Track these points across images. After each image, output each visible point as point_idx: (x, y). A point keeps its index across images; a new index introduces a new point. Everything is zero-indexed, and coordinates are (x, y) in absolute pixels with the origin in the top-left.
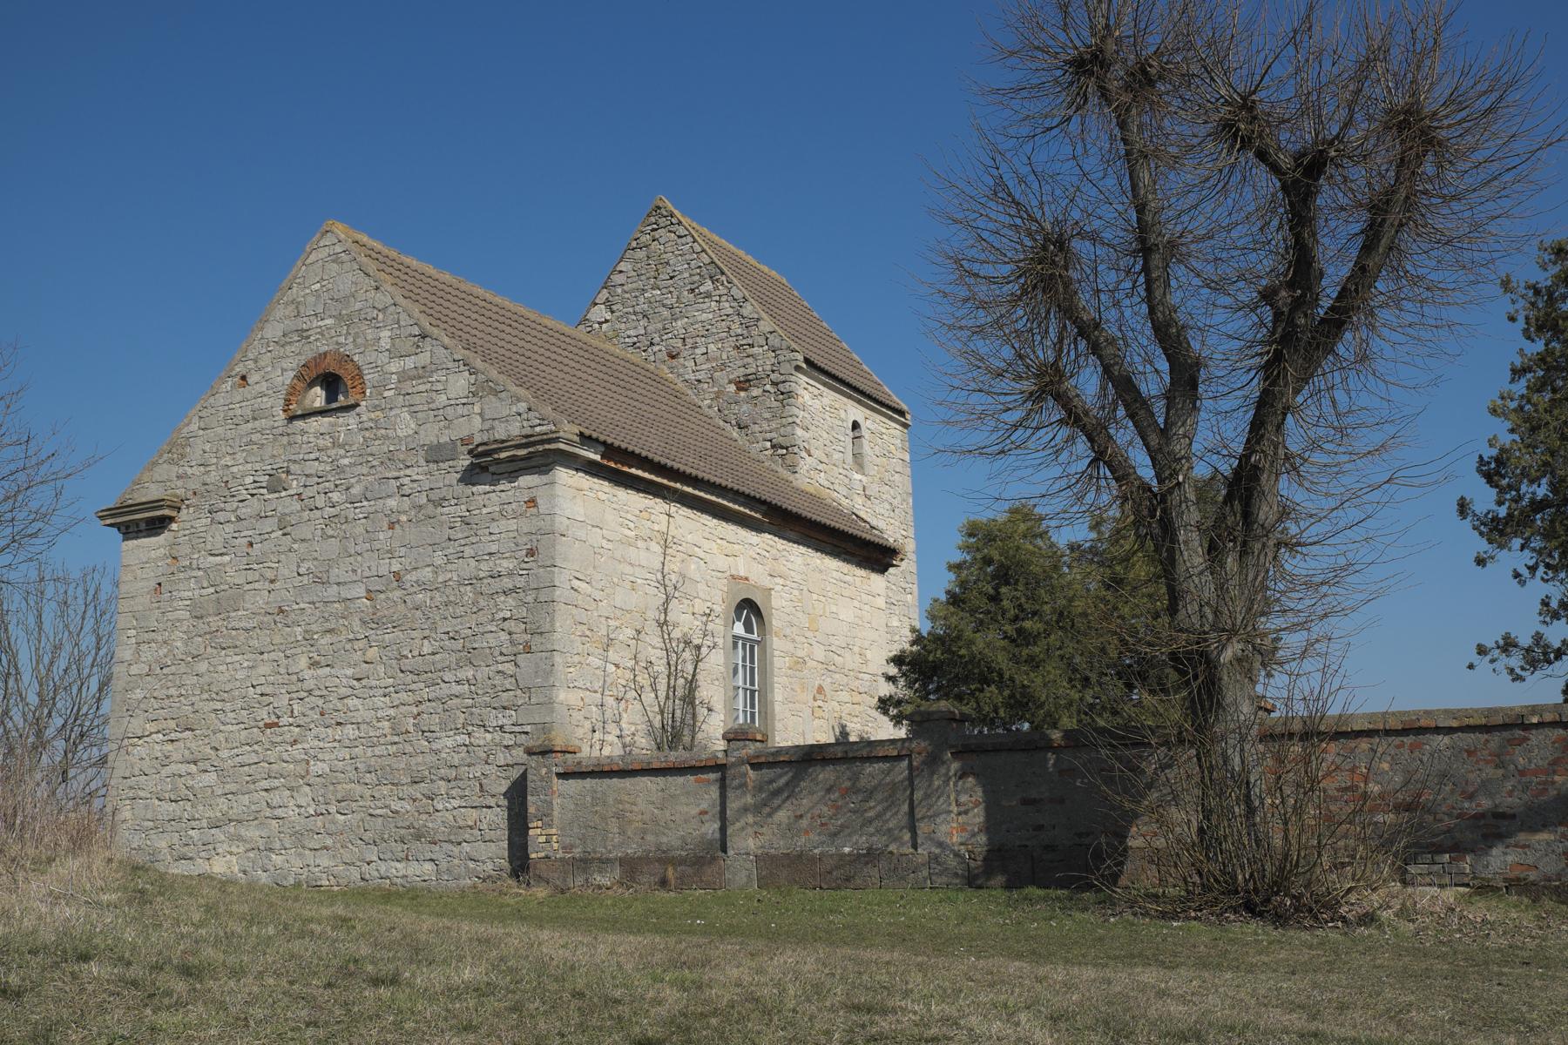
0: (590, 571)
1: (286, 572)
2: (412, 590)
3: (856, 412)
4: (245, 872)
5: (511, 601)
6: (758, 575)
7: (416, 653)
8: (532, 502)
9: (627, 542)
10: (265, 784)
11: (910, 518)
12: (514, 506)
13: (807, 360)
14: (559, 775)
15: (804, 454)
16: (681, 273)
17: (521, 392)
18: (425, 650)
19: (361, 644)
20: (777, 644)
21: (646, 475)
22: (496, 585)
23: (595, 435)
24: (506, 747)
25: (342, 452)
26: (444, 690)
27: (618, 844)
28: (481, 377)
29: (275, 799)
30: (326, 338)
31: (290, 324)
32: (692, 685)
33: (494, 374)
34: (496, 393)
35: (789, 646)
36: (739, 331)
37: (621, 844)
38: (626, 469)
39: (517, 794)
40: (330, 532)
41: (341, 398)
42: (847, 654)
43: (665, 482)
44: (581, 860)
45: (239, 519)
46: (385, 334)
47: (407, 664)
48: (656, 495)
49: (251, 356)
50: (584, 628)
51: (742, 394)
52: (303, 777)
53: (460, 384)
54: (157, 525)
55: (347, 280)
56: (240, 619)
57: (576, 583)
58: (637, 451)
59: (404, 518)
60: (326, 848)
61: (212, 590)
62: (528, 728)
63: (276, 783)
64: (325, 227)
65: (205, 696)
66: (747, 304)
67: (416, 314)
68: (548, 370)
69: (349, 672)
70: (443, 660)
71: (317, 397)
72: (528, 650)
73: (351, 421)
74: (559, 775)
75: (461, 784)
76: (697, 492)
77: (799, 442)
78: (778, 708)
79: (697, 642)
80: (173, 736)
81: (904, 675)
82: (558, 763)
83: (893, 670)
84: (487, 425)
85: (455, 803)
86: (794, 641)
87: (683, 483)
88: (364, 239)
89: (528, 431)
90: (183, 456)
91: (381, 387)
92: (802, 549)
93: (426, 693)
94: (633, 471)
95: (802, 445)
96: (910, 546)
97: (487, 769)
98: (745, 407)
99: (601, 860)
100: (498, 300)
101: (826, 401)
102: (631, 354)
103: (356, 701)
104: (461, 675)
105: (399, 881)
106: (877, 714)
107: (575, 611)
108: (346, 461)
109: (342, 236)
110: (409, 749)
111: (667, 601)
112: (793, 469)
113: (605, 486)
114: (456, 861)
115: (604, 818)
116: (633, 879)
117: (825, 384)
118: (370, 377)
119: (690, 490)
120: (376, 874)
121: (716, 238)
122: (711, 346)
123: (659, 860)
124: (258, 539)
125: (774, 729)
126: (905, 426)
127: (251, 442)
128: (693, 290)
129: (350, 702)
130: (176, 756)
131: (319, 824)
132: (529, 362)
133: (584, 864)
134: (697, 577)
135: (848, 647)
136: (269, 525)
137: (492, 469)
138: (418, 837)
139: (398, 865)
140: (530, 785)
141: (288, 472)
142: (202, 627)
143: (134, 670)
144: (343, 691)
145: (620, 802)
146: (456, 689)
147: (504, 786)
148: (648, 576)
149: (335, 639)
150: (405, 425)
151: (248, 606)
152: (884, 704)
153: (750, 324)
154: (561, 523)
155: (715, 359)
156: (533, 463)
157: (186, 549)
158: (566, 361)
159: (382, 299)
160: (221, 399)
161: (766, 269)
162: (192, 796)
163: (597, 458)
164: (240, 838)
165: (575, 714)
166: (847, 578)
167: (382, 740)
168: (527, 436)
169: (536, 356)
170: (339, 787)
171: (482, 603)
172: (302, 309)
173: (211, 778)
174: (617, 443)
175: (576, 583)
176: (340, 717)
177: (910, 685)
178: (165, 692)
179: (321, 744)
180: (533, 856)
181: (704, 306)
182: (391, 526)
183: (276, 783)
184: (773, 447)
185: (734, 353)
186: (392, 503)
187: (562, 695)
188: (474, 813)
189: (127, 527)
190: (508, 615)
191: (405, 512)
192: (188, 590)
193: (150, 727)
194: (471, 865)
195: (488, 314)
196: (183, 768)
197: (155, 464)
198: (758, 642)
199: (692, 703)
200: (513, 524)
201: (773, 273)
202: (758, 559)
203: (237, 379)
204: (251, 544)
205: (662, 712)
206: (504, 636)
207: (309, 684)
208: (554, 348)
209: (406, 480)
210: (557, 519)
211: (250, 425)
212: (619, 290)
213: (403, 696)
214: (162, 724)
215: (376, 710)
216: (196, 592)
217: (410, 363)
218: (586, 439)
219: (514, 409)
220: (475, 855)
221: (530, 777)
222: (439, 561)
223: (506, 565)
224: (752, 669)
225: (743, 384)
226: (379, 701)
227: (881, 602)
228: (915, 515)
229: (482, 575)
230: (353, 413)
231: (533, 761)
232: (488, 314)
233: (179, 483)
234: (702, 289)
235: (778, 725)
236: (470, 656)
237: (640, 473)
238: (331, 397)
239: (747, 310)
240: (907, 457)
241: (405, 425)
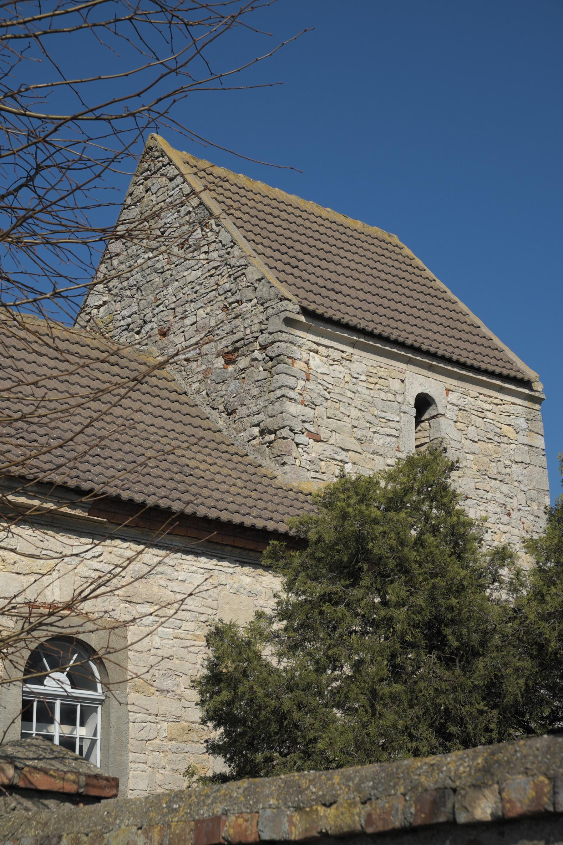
13: (304, 311)
36: (227, 286)
51: (231, 368)
98: (233, 385)
101: (356, 367)
112: (280, 459)
117: (354, 345)
128: (183, 244)
163: (86, 515)
240: (540, 442)
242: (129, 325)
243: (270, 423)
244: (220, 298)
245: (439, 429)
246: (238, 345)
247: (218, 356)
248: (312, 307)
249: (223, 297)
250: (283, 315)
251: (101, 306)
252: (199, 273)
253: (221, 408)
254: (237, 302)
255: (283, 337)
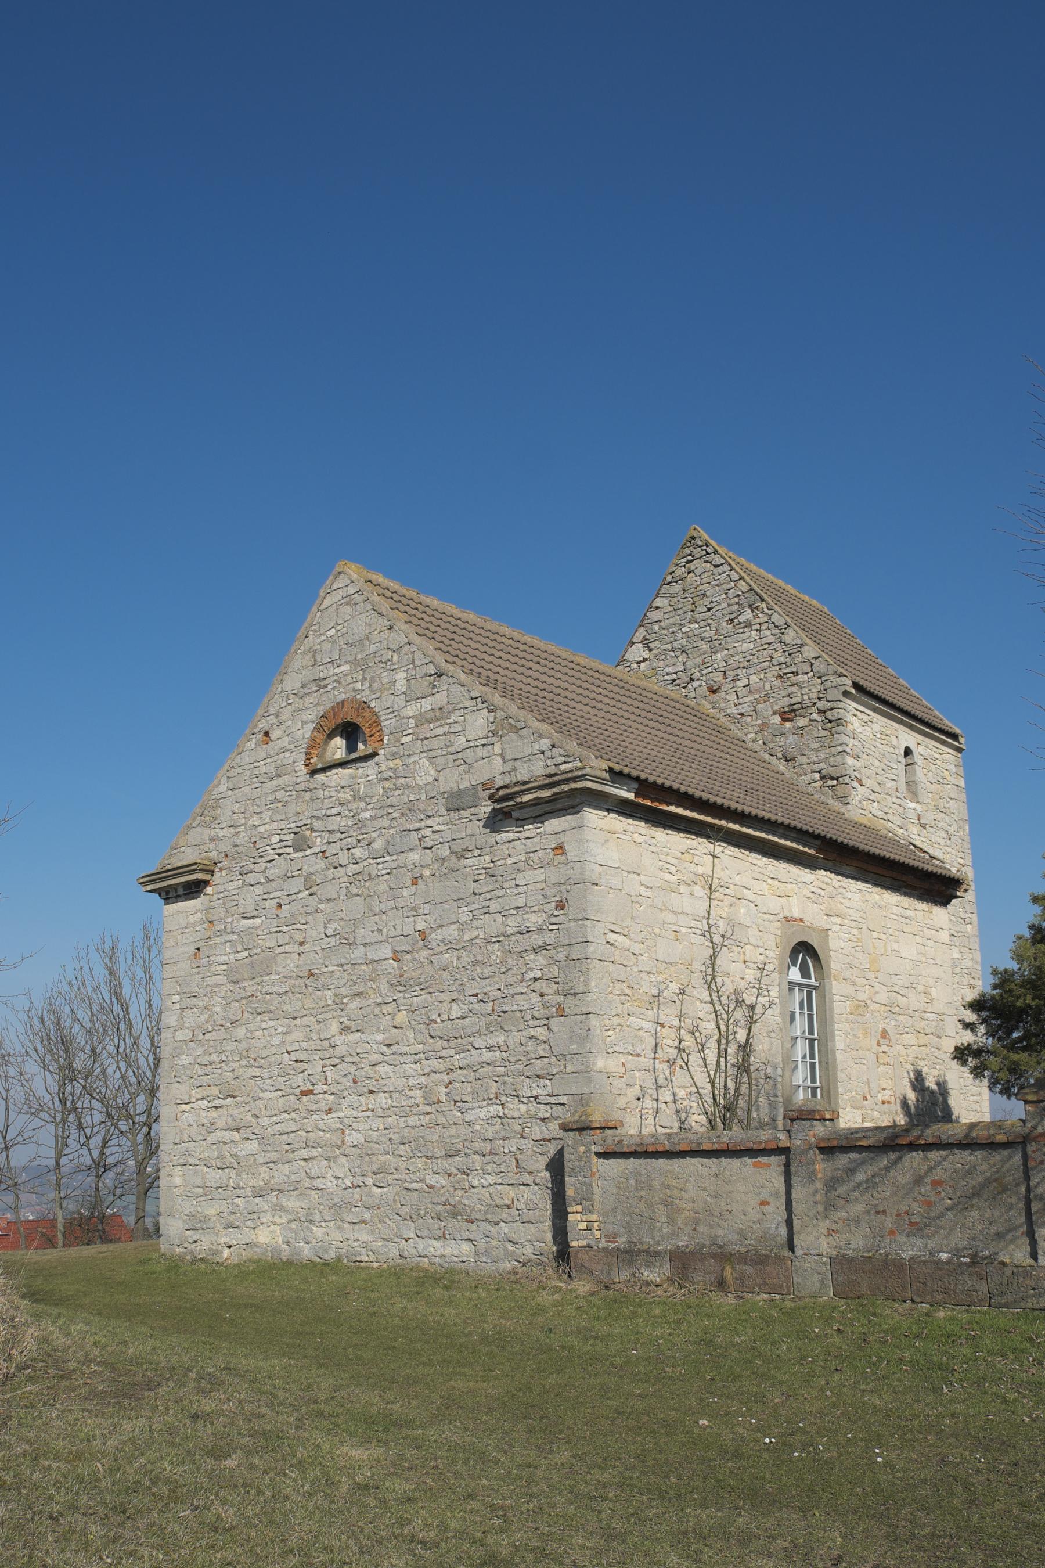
0: (628, 922)
1: (314, 934)
2: (438, 949)
3: (907, 737)
4: (288, 1243)
5: (541, 960)
6: (813, 915)
7: (444, 1017)
8: (560, 849)
9: (668, 888)
10: (303, 1153)
11: (967, 845)
12: (540, 854)
13: (856, 685)
14: (599, 1155)
15: (855, 784)
16: (718, 603)
17: (544, 727)
18: (455, 1014)
19: (389, 1009)
20: (836, 988)
21: (687, 813)
22: (526, 942)
23: (626, 770)
24: (542, 1120)
25: (362, 805)
26: (475, 1057)
27: (665, 1235)
28: (500, 714)
29: (314, 1168)
30: (345, 686)
31: (309, 674)
32: (745, 1049)
33: (513, 709)
34: (517, 730)
35: (849, 990)
36: (782, 659)
37: (671, 1235)
38: (664, 807)
39: (557, 1167)
40: (355, 891)
41: (361, 746)
42: (911, 994)
43: (709, 819)
44: (626, 1252)
45: (269, 880)
46: (401, 676)
47: (436, 1029)
48: (698, 834)
49: (272, 710)
50: (624, 986)
51: (788, 725)
52: (339, 1147)
53: (479, 723)
54: (194, 889)
55: (361, 622)
56: (272, 983)
57: (612, 937)
58: (675, 786)
59: (427, 873)
60: (363, 1222)
61: (246, 954)
62: (564, 1100)
63: (314, 1152)
64: (338, 569)
65: (244, 1062)
66: (790, 630)
67: (431, 651)
68: (579, 706)
69: (379, 1037)
70: (472, 1024)
71: (338, 748)
72: (561, 1013)
73: (370, 771)
74: (599, 1155)
75: (496, 1159)
76: (744, 830)
77: (850, 772)
78: (839, 1056)
79: (750, 1000)
80: (217, 1103)
81: (984, 1021)
82: (596, 1142)
83: (971, 1017)
84: (509, 766)
85: (491, 1179)
86: (854, 984)
87: (714, 817)
88: (380, 578)
89: (552, 770)
90: (215, 818)
91: (401, 732)
92: (860, 885)
93: (458, 1060)
94: (672, 809)
95: (853, 774)
96: (969, 873)
97: (524, 1144)
98: (791, 739)
99: (648, 1252)
100: (526, 638)
101: (876, 727)
102: (671, 691)
103: (388, 1068)
104: (492, 1040)
105: (437, 1260)
106: (955, 1064)
107: (611, 968)
108: (367, 815)
109: (355, 576)
110: (441, 1120)
111: (713, 957)
112: (844, 800)
113: (640, 828)
114: (495, 1243)
115: (650, 1205)
116: (684, 1276)
118: (388, 723)
119: (736, 827)
120: (414, 1251)
121: (753, 567)
122: (753, 678)
123: (714, 1256)
124: (286, 900)
125: (836, 1081)
126: (959, 750)
127: (275, 801)
128: (732, 620)
129: (382, 1069)
130: (220, 1124)
131: (357, 1196)
132: (557, 699)
133: (630, 1255)
134: (747, 921)
135: (912, 986)
136: (296, 885)
137: (515, 814)
138: (454, 1215)
139: (436, 1244)
140: (568, 1165)
141: (312, 829)
142: (239, 992)
143: (179, 1036)
144: (375, 1058)
145: (668, 1187)
146: (487, 1056)
147: (542, 1162)
148: (693, 924)
149: (364, 1003)
150: (424, 772)
151: (280, 969)
152: (961, 1054)
153: (793, 651)
154: (592, 871)
155: (758, 691)
156: (559, 805)
157: (220, 913)
158: (600, 698)
159: (397, 638)
160: (246, 758)
161: (807, 598)
162: (237, 1164)
163: (631, 796)
164: (282, 1208)
165: (616, 1082)
166: (909, 913)
167: (415, 1110)
168: (551, 776)
169: (567, 693)
170: (374, 1158)
171: (511, 962)
172: (318, 657)
173: (253, 1146)
174: (651, 779)
175: (612, 937)
176: (371, 1085)
177: (989, 1034)
178: (207, 1058)
179: (355, 1113)
180: (574, 1244)
181: (745, 636)
182: (415, 883)
183: (314, 1152)
184: (822, 778)
185: (777, 683)
186: (414, 857)
187: (601, 1063)
188: (511, 1192)
189: (167, 893)
190: (539, 974)
191: (427, 866)
192: (225, 955)
193: (196, 1093)
194: (510, 1247)
195: (514, 652)
196: (227, 1136)
197: (189, 827)
198: (816, 987)
199: (747, 1071)
200: (540, 875)
201: (814, 602)
202: (813, 898)
203: (260, 736)
204: (280, 906)
205: (712, 1083)
206: (535, 998)
207: (341, 1050)
208: (585, 685)
209: (427, 832)
210: (588, 866)
211: (274, 782)
212: (656, 627)
213: (434, 1063)
214: (208, 1091)
215: (407, 1077)
216: (232, 956)
217: (426, 704)
218: (617, 776)
219: (537, 746)
220: (513, 1236)
221: (567, 1156)
222: (464, 918)
223: (534, 920)
224: (811, 1017)
225: (788, 715)
226: (410, 1069)
227: (944, 936)
228: (972, 842)
229: (510, 931)
230: (371, 763)
231: (570, 1138)
232: (514, 652)
233: (212, 846)
234: (741, 619)
235: (841, 1075)
236: (499, 1020)
237: (680, 811)
238: (351, 748)
239: (790, 636)
240: (962, 783)
241: (424, 772)
242: (674, 681)
243: (832, 771)
244: (773, 668)
245: (915, 775)
246: (795, 707)
247: (774, 713)
248: (862, 682)
249: (777, 668)
250: (843, 688)
251: (641, 662)
252: (751, 646)
253: (780, 755)
254: (793, 673)
255: (841, 705)
